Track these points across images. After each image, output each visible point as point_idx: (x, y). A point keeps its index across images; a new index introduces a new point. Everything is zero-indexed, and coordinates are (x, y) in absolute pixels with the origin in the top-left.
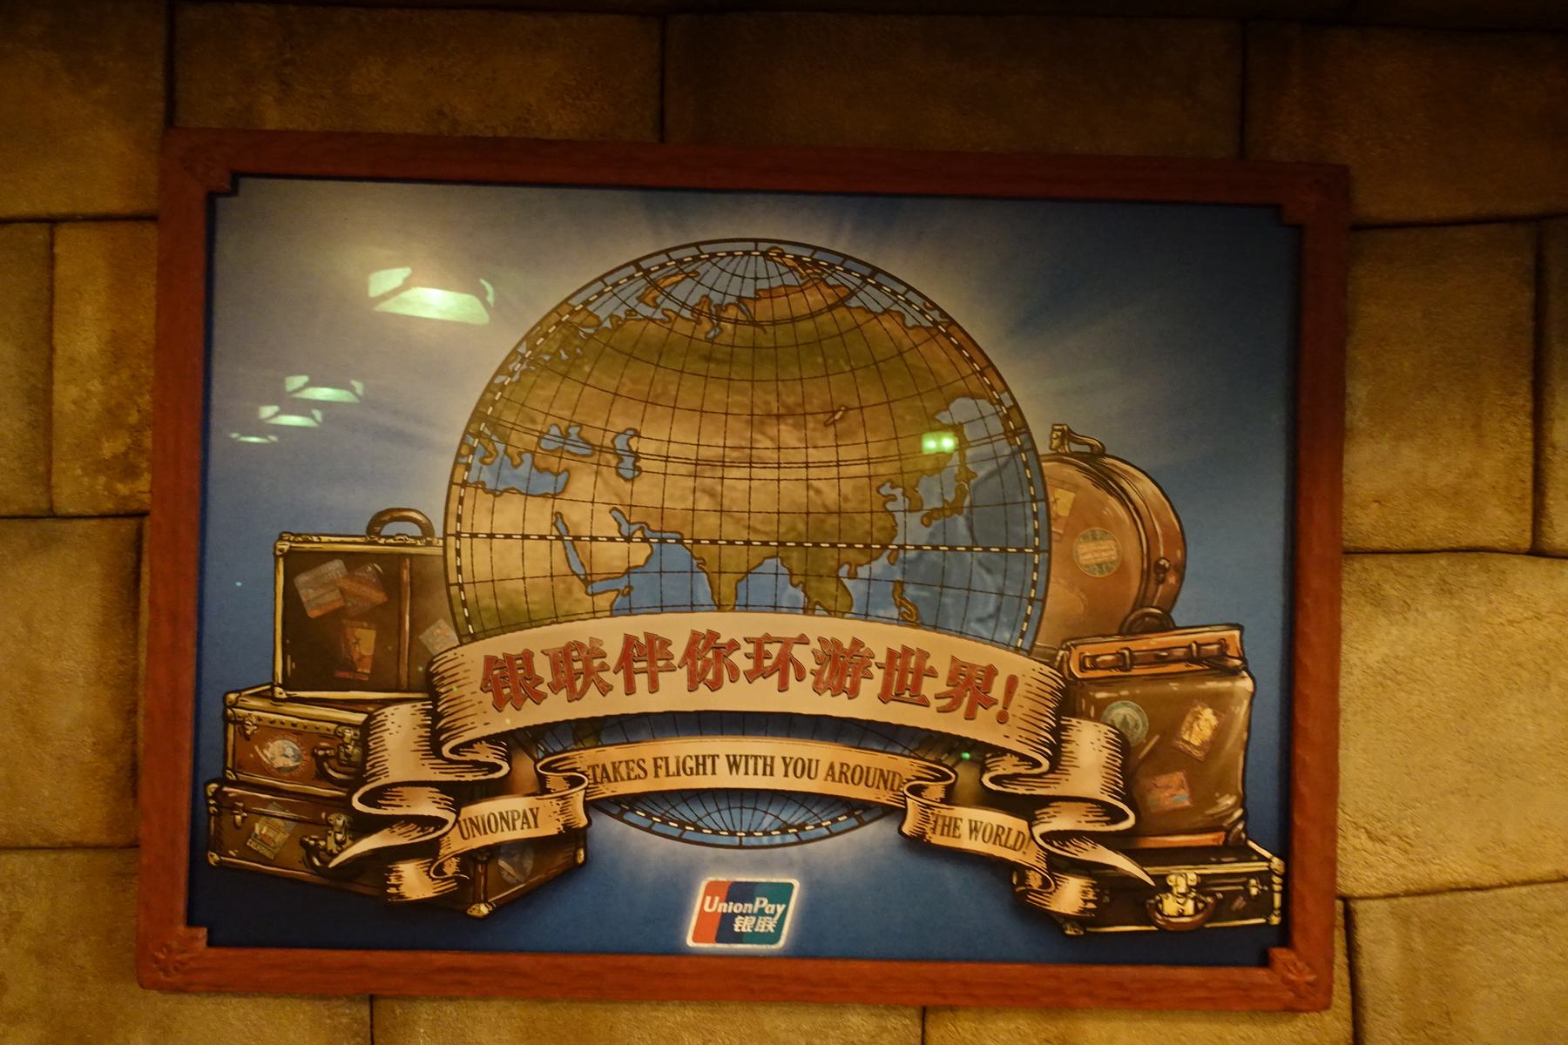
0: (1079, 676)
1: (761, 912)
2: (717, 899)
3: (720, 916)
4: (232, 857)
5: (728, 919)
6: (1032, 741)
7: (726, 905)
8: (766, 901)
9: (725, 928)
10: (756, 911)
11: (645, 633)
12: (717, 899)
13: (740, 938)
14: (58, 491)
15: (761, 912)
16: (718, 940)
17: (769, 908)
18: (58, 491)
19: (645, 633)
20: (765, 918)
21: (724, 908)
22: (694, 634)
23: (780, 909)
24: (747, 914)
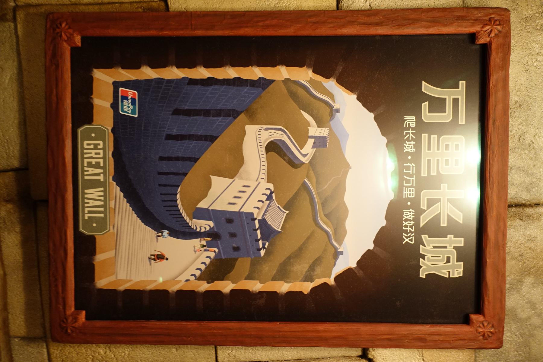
0: (313, 78)
1: (129, 107)
2: (132, 95)
3: (127, 96)
4: (129, 113)
5: (127, 98)
6: (127, 274)
7: (130, 98)
8: (132, 108)
9: (125, 98)
10: (129, 106)
11: (312, 148)
12: (132, 95)
13: (122, 102)
14: (189, 348)
15: (129, 107)
16: (121, 96)
17: (130, 109)
18: (189, 348)
19: (312, 148)
20: (127, 108)
21: (130, 97)
22: (226, 219)
23: (130, 112)
24: (128, 103)
